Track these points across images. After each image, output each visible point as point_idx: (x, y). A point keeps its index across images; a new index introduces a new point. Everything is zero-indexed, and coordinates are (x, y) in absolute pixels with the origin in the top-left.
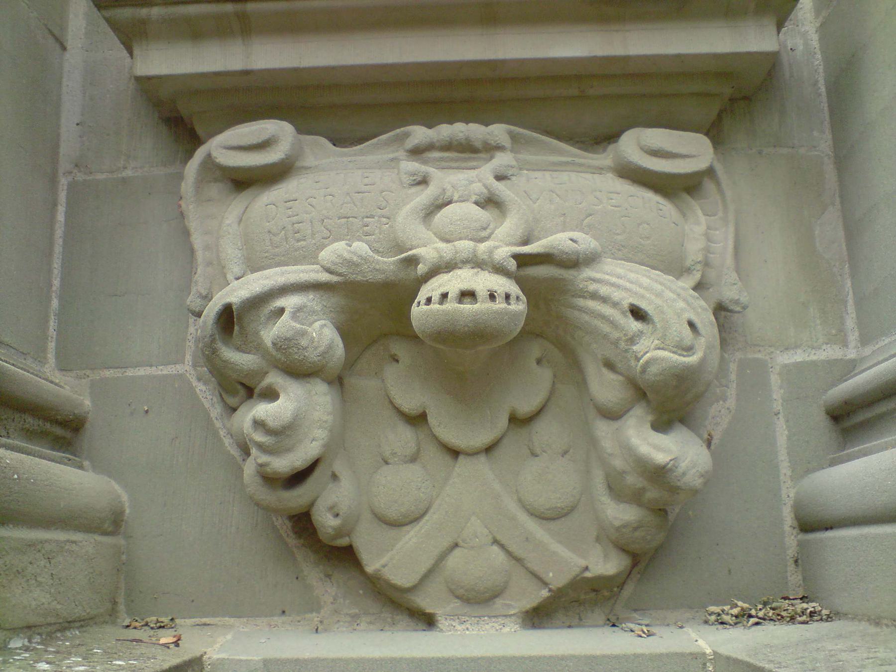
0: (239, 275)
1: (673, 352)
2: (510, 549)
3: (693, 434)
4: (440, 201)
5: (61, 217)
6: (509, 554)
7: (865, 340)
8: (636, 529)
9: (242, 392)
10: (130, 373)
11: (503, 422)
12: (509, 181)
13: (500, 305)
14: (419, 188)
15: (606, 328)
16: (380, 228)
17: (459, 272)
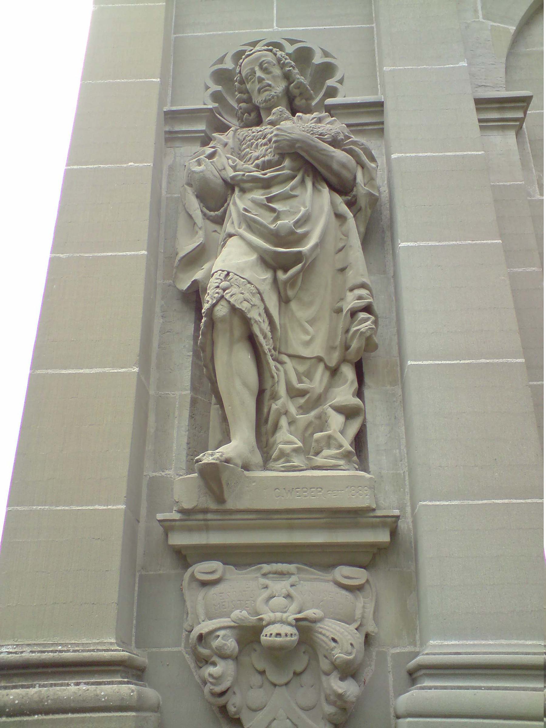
0: (203, 620)
1: (345, 655)
2: (293, 721)
3: (355, 682)
4: (272, 596)
5: (136, 588)
6: (292, 722)
8: (334, 715)
9: (204, 662)
10: (162, 650)
11: (291, 675)
12: (295, 587)
14: (265, 589)
15: (324, 645)
16: (251, 605)
17: (276, 625)
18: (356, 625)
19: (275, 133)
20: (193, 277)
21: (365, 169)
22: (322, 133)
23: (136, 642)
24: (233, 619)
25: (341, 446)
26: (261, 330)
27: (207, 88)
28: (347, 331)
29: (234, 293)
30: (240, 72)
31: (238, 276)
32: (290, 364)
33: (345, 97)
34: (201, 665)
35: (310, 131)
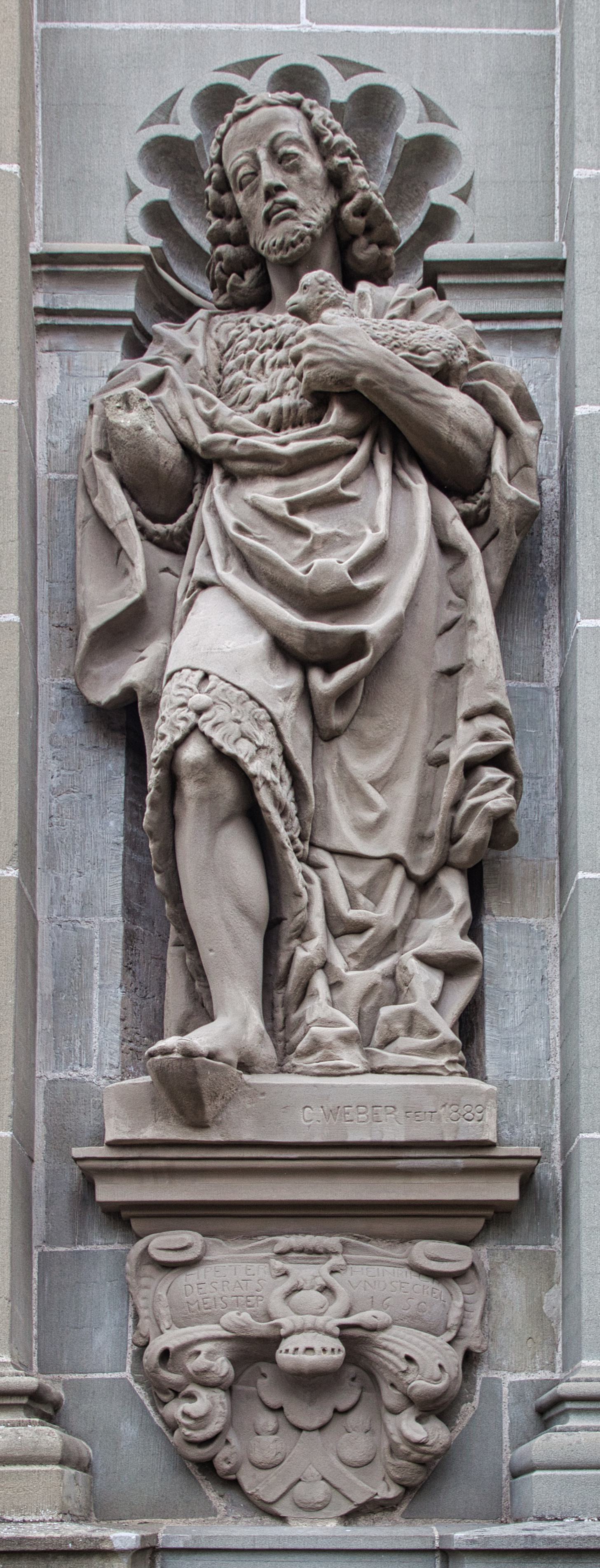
7: (564, 1369)
9: (172, 1394)
10: (89, 1376)
11: (329, 1413)
13: (328, 1356)
15: (391, 1366)
18: (450, 1336)
19: (310, 340)
20: (122, 674)
21: (511, 439)
22: (418, 347)
23: (39, 1365)
24: (224, 1326)
25: (434, 1032)
26: (278, 803)
27: (134, 191)
28: (456, 805)
29: (220, 721)
30: (219, 160)
31: (227, 682)
32: (333, 870)
33: (471, 240)
34: (164, 1398)
35: (390, 338)
